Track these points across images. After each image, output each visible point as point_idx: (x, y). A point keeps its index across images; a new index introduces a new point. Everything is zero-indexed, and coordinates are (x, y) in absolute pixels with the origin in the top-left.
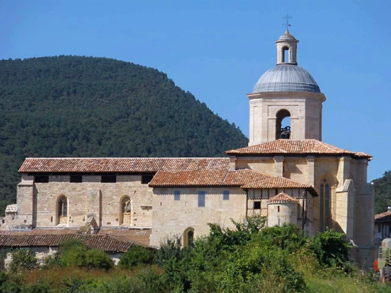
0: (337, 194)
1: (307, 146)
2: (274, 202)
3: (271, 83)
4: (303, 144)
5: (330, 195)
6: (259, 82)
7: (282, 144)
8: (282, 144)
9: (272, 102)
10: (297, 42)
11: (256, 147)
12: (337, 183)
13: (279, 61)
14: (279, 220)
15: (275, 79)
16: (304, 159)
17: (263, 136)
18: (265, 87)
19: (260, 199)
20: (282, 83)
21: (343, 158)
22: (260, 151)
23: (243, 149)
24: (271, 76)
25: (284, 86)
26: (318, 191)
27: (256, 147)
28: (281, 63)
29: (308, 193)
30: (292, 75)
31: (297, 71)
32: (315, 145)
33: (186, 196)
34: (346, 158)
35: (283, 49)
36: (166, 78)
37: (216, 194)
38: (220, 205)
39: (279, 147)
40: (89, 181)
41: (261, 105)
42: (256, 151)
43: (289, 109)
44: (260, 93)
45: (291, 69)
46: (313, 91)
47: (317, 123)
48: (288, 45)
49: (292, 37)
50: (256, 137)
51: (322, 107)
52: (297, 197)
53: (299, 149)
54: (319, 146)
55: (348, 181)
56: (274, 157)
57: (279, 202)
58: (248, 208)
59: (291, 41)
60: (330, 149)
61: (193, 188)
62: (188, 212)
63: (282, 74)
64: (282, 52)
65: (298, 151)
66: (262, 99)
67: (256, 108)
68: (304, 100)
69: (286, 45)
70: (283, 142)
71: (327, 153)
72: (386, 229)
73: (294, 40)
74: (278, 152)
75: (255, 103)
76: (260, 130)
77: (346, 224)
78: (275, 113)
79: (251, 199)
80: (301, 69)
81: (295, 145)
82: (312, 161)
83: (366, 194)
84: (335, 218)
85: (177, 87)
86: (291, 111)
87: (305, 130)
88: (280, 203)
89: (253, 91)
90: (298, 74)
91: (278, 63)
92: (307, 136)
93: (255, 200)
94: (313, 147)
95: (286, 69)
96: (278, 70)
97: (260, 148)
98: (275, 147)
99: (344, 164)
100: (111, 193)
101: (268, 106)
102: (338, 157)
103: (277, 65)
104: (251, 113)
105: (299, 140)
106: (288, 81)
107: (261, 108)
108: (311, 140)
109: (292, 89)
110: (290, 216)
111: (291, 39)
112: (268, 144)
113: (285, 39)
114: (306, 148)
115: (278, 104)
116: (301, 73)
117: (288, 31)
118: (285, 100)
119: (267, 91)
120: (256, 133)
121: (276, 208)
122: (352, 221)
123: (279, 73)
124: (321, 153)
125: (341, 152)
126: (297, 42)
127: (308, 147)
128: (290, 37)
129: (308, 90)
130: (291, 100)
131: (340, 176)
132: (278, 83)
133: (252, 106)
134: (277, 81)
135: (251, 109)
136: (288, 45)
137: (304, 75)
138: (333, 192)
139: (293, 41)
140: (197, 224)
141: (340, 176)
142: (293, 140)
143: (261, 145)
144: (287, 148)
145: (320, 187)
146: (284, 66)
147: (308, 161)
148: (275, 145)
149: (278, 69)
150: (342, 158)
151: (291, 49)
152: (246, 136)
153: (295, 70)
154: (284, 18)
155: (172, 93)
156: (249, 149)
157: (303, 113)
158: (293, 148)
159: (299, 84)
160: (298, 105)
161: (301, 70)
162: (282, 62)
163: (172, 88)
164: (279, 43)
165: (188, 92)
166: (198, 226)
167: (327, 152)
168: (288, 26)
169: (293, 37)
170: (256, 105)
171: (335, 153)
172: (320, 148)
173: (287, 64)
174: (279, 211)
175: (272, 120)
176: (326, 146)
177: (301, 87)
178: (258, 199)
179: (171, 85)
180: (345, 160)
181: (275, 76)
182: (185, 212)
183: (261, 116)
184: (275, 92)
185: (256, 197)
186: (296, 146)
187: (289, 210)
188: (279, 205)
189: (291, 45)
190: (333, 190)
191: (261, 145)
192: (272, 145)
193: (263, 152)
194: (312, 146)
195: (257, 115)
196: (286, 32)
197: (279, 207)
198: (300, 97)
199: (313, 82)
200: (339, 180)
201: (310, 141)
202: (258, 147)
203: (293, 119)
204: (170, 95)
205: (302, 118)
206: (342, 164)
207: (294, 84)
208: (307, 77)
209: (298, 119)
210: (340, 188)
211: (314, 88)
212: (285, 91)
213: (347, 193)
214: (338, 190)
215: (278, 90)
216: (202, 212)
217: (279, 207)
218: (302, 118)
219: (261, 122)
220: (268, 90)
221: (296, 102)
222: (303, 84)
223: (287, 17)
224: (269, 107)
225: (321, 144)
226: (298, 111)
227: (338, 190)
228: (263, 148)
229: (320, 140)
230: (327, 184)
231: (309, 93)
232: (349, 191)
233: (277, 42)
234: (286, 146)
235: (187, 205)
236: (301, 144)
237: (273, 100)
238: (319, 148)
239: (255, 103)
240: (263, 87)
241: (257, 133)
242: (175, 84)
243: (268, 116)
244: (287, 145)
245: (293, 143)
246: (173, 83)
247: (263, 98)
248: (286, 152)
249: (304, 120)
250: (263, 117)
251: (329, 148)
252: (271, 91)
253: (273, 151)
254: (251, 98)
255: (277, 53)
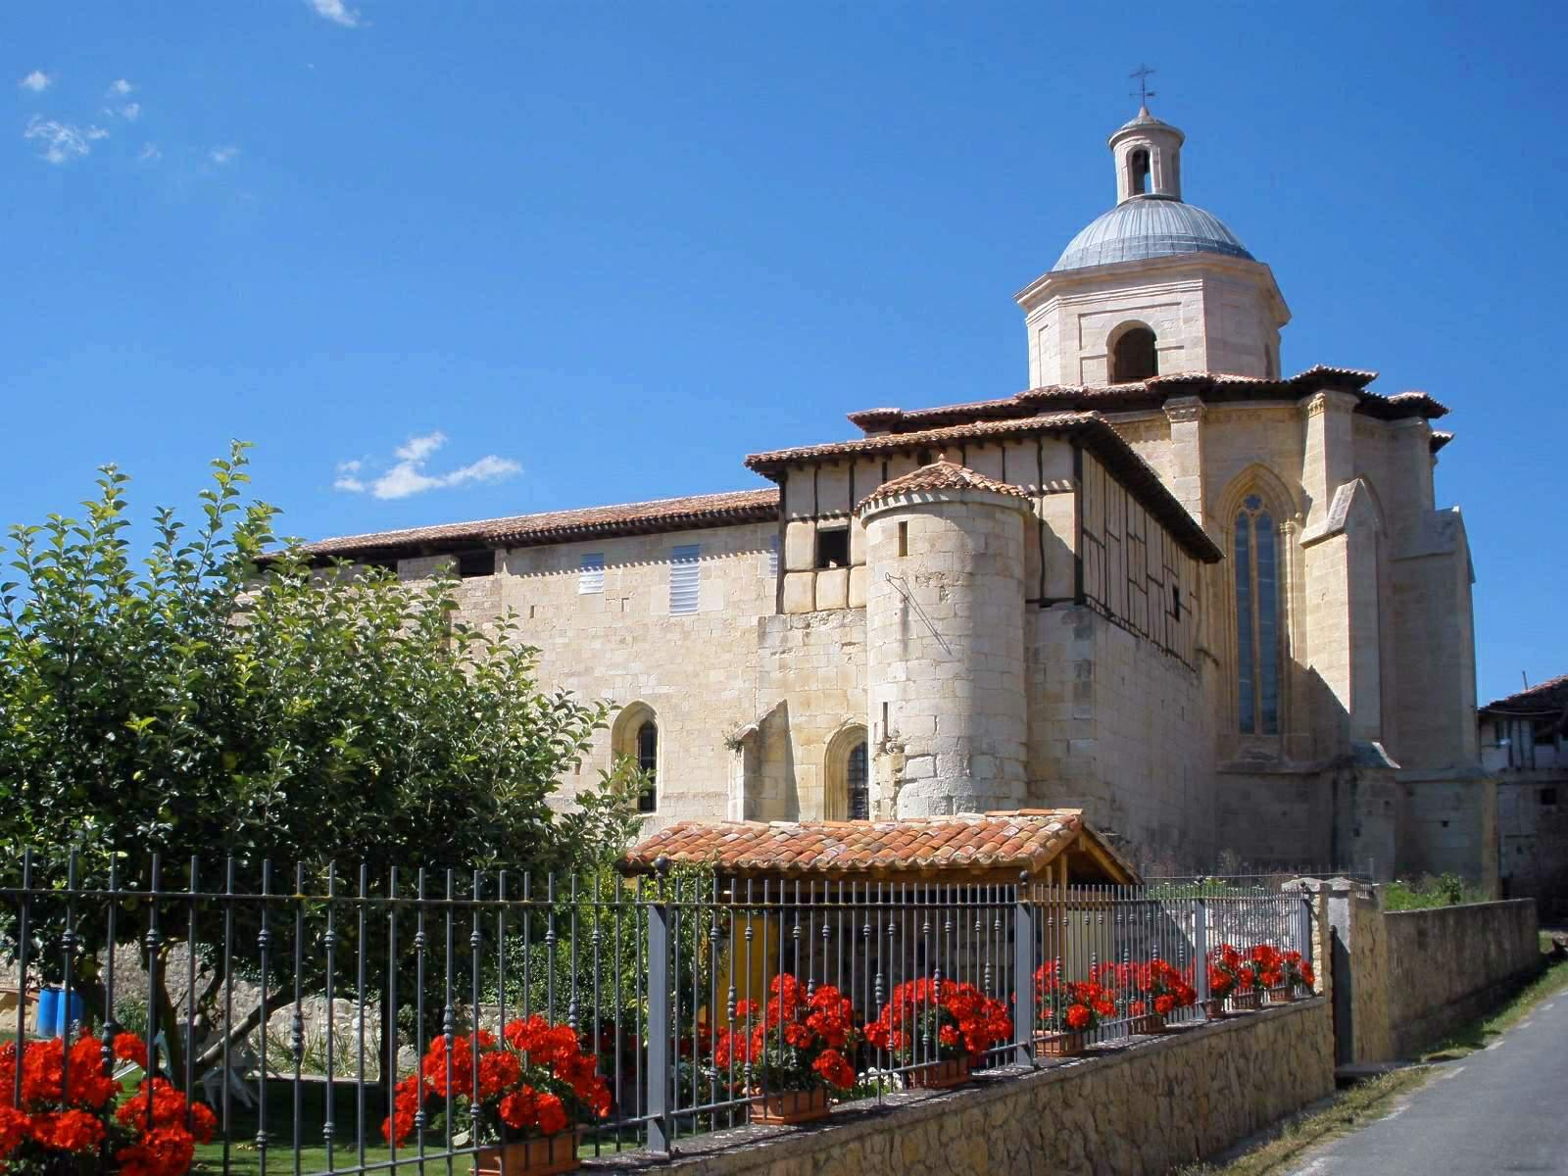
0: (1308, 550)
2: (882, 507)
5: (1276, 561)
9: (1091, 302)
12: (1305, 503)
14: (905, 599)
19: (845, 515)
21: (1318, 395)
26: (1218, 539)
29: (1086, 455)
33: (624, 575)
34: (1333, 395)
35: (1131, 158)
37: (743, 554)
38: (756, 599)
40: (415, 579)
52: (1033, 488)
55: (1345, 491)
57: (903, 501)
58: (788, 566)
59: (1153, 130)
61: (653, 537)
62: (629, 639)
68: (1200, 283)
69: (1139, 143)
72: (1520, 731)
77: (1195, 480)
79: (804, 520)
82: (1191, 418)
83: (1434, 555)
84: (1304, 654)
88: (911, 508)
93: (822, 524)
99: (1327, 420)
100: (479, 612)
101: (1081, 316)
104: (1033, 353)
110: (971, 574)
115: (1110, 306)
118: (1135, 290)
121: (891, 538)
122: (1371, 657)
130: (1151, 288)
131: (1313, 475)
138: (1288, 546)
140: (664, 690)
141: (1313, 475)
145: (1233, 527)
147: (1174, 417)
150: (1317, 399)
157: (1199, 328)
160: (1179, 304)
166: (668, 697)
174: (903, 552)
177: (1189, 247)
178: (836, 517)
180: (1327, 405)
182: (619, 638)
185: (824, 510)
187: (963, 545)
188: (903, 518)
190: (1288, 536)
197: (903, 526)
198: (1186, 276)
200: (1310, 493)
206: (1316, 424)
209: (1181, 347)
210: (1318, 523)
213: (1341, 540)
214: (1310, 532)
216: (686, 635)
217: (903, 526)
221: (1170, 292)
223: (1143, 72)
224: (1083, 320)
227: (1310, 532)
230: (1263, 515)
232: (1351, 526)
235: (627, 609)
237: (1094, 296)
243: (1081, 348)
250: (1063, 352)
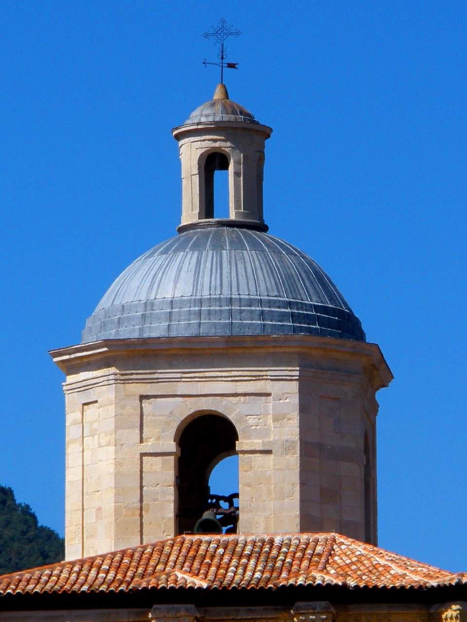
1: (301, 560)
3: (152, 304)
4: (286, 554)
6: (105, 302)
7: (191, 553)
8: (191, 553)
9: (157, 381)
10: (265, 133)
11: (76, 569)
13: (190, 213)
15: (171, 285)
16: (286, 614)
17: (121, 529)
18: (129, 319)
20: (201, 302)
21: (454, 607)
22: (91, 586)
23: (16, 576)
24: (153, 273)
25: (209, 312)
27: (76, 569)
28: (195, 220)
30: (241, 270)
31: (263, 251)
32: (336, 558)
36: (9, 502)
39: (178, 566)
41: (112, 396)
42: (82, 585)
43: (232, 411)
44: (107, 343)
45: (237, 245)
46: (332, 334)
47: (354, 470)
48: (226, 146)
49: (242, 113)
50: (89, 537)
51: (375, 411)
53: (263, 572)
54: (354, 559)
56: (151, 607)
59: (236, 128)
60: (400, 571)
63: (199, 262)
64: (199, 173)
65: (259, 580)
66: (113, 370)
67: (90, 410)
69: (217, 144)
70: (199, 546)
71: (385, 587)
73: (252, 126)
74: (171, 585)
75: (86, 387)
76: (107, 501)
78: (172, 432)
80: (282, 246)
81: (249, 557)
85: (43, 529)
86: (242, 418)
87: (302, 501)
89: (80, 338)
90: (269, 263)
91: (184, 222)
92: (308, 523)
94: (327, 561)
95: (218, 246)
96: (184, 250)
97: (93, 572)
98: (160, 567)
101: (142, 398)
102: (436, 606)
103: (182, 229)
104: (72, 432)
105: (267, 538)
106: (226, 294)
107: (112, 410)
108: (321, 536)
109: (242, 326)
111: (236, 122)
112: (132, 556)
113: (211, 119)
114: (295, 568)
116: (281, 261)
117: (224, 87)
119: (136, 335)
120: (90, 519)
123: (187, 260)
124: (357, 587)
125: (447, 583)
126: (265, 133)
127: (305, 563)
128: (234, 112)
129: (310, 330)
130: (236, 372)
132: (182, 303)
133: (72, 401)
134: (178, 294)
135: (72, 417)
136: (226, 146)
137: (294, 271)
139: (244, 129)
142: (241, 538)
143: (98, 561)
144: (213, 569)
146: (209, 233)
148: (163, 558)
149: (182, 247)
151: (237, 163)
152: (61, 536)
153: (255, 246)
154: (207, 36)
155: (27, 547)
156: (44, 578)
157: (291, 429)
158: (240, 571)
159: (270, 303)
160: (269, 395)
161: (277, 248)
162: (200, 218)
163: (27, 531)
164: (186, 140)
165: (34, 512)
167: (385, 581)
168: (227, 70)
169: (249, 115)
170: (92, 395)
171: (420, 587)
172: (359, 569)
173: (221, 224)
175: (159, 459)
176: (382, 562)
177: (282, 317)
179: (26, 522)
181: (172, 272)
183: (113, 440)
184: (170, 340)
186: (252, 562)
189: (237, 146)
191: (98, 561)
192: (149, 559)
193: (103, 588)
194: (323, 560)
195: (96, 437)
196: (218, 95)
199: (332, 299)
201: (317, 542)
202: (86, 567)
203: (247, 456)
204: (19, 554)
205: (287, 448)
207: (251, 302)
208: (309, 279)
209: (269, 452)
211: (338, 325)
212: (212, 332)
215: (182, 329)
218: (287, 448)
219: (112, 469)
220: (141, 330)
221: (258, 378)
222: (289, 304)
223: (222, 32)
224: (146, 404)
225: (364, 552)
226: (270, 421)
228: (107, 572)
229: (370, 538)
231: (316, 340)
233: (179, 137)
234: (207, 560)
236: (274, 552)
238: (354, 567)
239: (86, 387)
240: (119, 319)
241: (94, 520)
242: (39, 519)
243: (141, 441)
244: (213, 557)
245: (238, 549)
246: (34, 517)
247: (117, 367)
248: (205, 585)
249: (294, 459)
251: (396, 570)
252: (154, 335)
253: (148, 582)
254: (72, 367)
255: (180, 180)
